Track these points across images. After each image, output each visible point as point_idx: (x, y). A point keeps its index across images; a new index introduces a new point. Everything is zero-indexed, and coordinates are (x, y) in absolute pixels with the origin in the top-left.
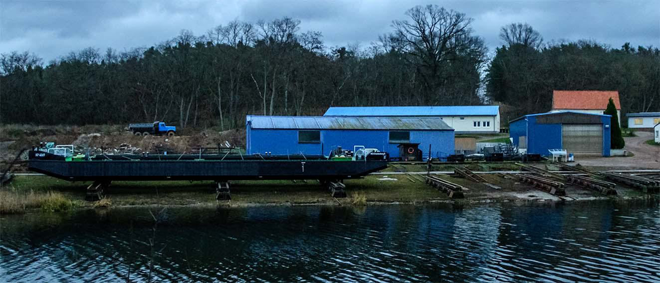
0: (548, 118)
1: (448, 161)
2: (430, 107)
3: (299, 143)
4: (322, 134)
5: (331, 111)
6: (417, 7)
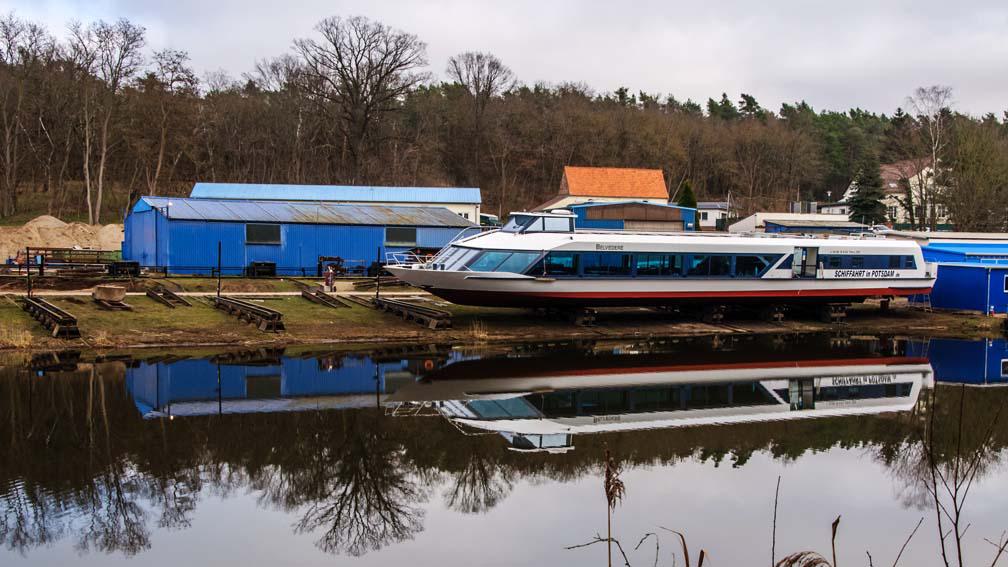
0: (606, 211)
1: (853, 219)
2: (370, 187)
3: (248, 244)
4: (283, 230)
5: (201, 189)
6: (403, 42)
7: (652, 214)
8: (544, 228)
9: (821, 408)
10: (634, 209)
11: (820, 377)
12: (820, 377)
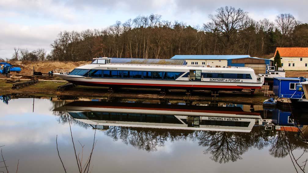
0: (238, 60)
7: (254, 61)
8: (97, 62)
9: (202, 127)
10: (248, 60)
11: (202, 116)
12: (202, 116)
